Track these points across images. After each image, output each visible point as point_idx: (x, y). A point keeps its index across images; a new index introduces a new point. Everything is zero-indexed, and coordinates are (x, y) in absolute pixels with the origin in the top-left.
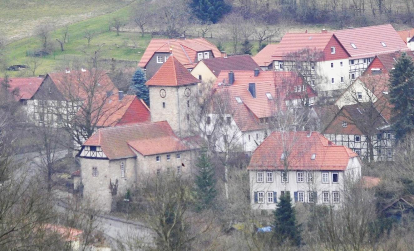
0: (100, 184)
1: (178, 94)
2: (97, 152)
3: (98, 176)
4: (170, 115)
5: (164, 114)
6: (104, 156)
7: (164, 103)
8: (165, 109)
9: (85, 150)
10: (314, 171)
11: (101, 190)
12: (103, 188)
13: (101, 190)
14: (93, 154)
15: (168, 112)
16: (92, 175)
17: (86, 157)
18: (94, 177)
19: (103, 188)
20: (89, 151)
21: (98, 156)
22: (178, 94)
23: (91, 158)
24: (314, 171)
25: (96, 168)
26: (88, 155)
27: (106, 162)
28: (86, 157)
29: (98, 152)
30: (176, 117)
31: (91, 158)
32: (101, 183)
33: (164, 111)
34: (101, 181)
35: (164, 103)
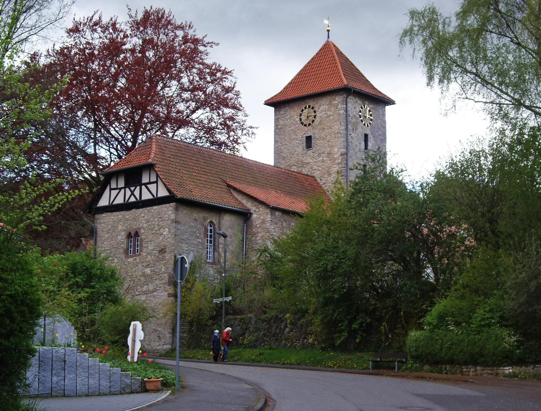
0: (144, 275)
1: (346, 111)
2: (143, 187)
3: (140, 255)
4: (323, 161)
5: (309, 163)
6: (163, 193)
7: (309, 139)
8: (310, 152)
9: (111, 189)
10: (52, 383)
11: (145, 293)
12: (151, 287)
13: (145, 293)
14: (132, 193)
15: (319, 155)
16: (123, 256)
17: (112, 208)
18: (130, 260)
19: (151, 287)
20: (120, 189)
21: (146, 196)
22: (346, 111)
23: (126, 207)
24: (52, 383)
25: (137, 234)
26: (120, 200)
27: (168, 210)
28: (112, 208)
29: (145, 184)
30: (338, 164)
31: (126, 207)
32: (148, 271)
33: (309, 157)
34: (148, 266)
35: (309, 139)
